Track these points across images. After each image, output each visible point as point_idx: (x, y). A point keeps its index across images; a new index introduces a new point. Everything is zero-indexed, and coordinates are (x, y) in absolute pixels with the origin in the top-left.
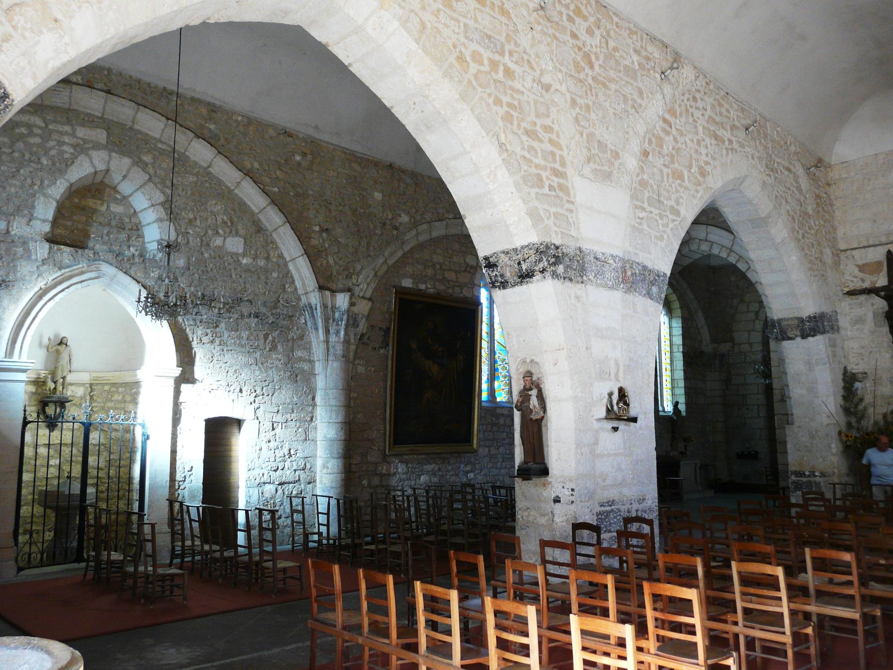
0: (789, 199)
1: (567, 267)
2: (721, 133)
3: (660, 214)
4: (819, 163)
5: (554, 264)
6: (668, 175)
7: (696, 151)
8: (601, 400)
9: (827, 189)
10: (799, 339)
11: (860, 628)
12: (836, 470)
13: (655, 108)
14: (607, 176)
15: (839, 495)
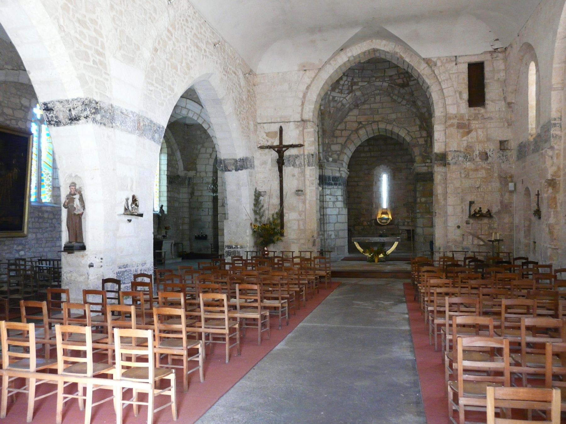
0: (234, 90)
1: (103, 116)
2: (200, 44)
3: (162, 89)
4: (251, 72)
5: (94, 113)
6: (168, 65)
7: (186, 54)
8: (121, 203)
9: (254, 87)
10: (234, 171)
11: (259, 323)
12: (248, 245)
13: (163, 22)
14: (132, 60)
15: (249, 258)
